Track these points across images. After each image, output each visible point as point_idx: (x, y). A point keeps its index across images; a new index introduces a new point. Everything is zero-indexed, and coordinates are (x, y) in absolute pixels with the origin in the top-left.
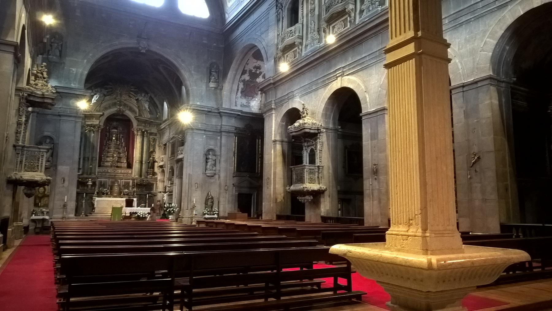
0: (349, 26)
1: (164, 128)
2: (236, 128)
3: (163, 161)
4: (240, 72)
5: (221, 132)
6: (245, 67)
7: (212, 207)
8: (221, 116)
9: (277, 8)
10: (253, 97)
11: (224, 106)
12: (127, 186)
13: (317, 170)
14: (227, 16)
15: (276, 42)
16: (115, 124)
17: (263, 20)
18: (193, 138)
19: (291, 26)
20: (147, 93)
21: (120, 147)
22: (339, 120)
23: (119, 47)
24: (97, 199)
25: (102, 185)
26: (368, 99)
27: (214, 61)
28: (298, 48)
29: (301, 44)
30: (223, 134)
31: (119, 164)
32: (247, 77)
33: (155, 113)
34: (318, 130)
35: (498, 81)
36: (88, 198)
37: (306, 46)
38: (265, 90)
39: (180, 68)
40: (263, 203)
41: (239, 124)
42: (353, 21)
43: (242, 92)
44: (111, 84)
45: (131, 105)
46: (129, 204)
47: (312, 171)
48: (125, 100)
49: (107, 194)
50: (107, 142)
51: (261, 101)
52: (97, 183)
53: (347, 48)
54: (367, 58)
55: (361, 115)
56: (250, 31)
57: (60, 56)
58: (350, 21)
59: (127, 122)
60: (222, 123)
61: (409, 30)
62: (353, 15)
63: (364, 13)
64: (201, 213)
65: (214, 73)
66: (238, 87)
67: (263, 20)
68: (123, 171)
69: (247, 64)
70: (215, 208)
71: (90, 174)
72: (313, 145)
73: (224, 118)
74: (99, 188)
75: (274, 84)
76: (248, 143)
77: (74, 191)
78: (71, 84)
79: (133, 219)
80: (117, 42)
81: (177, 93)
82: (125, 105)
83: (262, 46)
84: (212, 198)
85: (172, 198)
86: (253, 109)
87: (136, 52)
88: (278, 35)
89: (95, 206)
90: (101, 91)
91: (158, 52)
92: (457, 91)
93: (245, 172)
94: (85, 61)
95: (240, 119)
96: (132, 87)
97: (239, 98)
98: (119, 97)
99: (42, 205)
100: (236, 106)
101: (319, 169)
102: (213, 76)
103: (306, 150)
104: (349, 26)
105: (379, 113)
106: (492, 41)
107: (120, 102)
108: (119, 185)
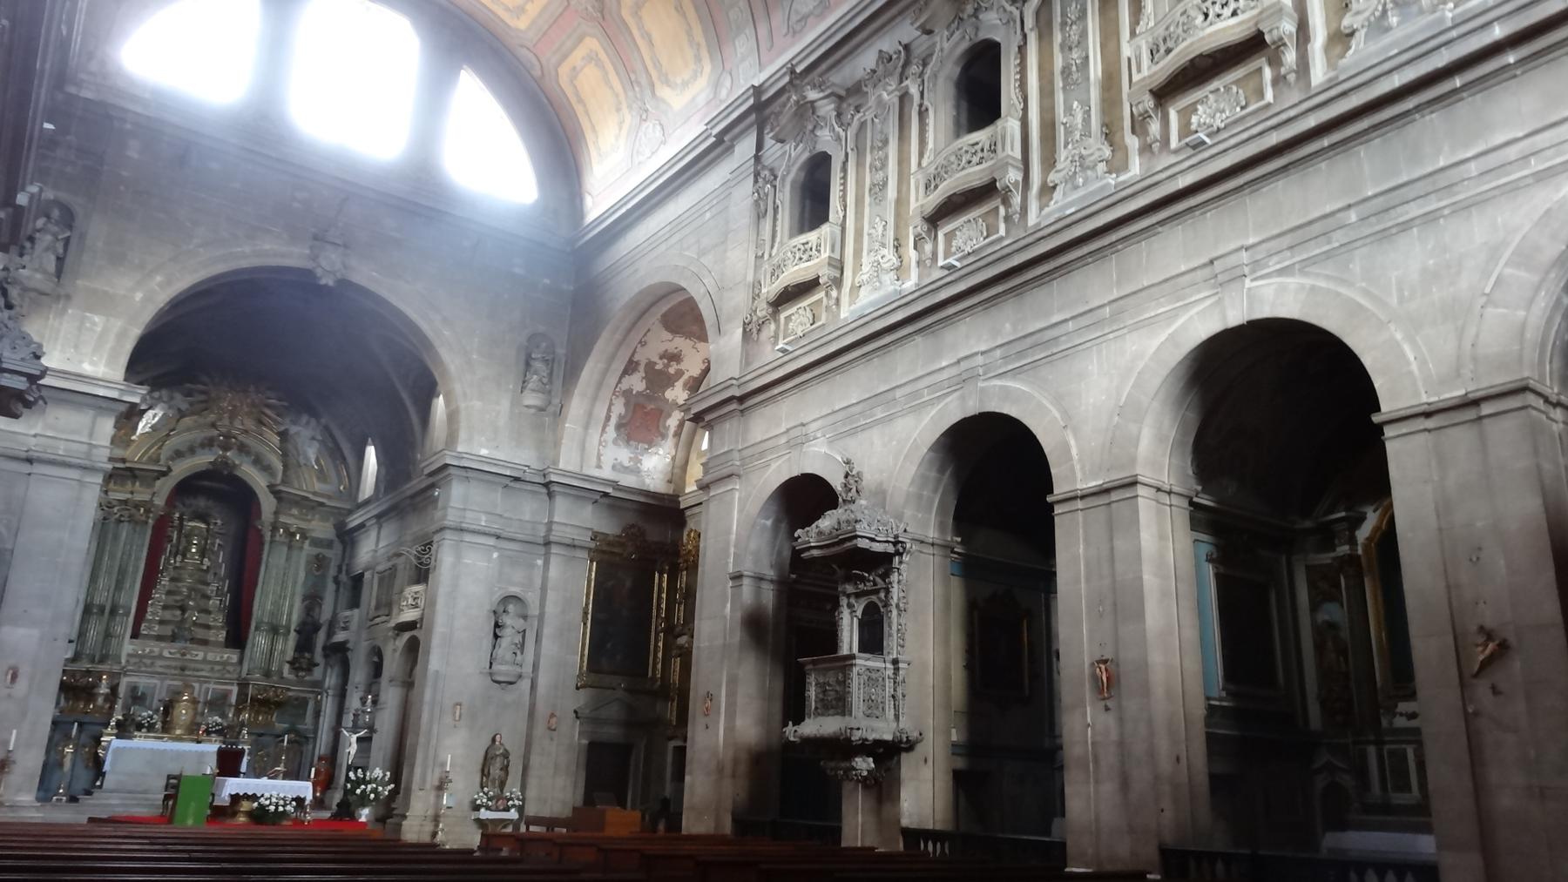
0: (1002, 232)
1: (362, 526)
3: (416, 606)
4: (619, 366)
5: (547, 544)
7: (502, 785)
8: (550, 495)
9: (756, 181)
10: (651, 444)
11: (561, 466)
13: (890, 672)
14: (588, 201)
15: (750, 278)
16: (201, 503)
17: (708, 215)
18: (458, 557)
19: (802, 231)
20: (313, 413)
22: (957, 518)
25: (137, 697)
26: (1074, 452)
27: (541, 328)
28: (827, 294)
29: (838, 282)
31: (200, 633)
32: (637, 383)
35: (1159, 490)
36: (84, 738)
37: (856, 289)
38: (707, 418)
39: (437, 343)
40: (687, 778)
41: (609, 526)
42: (1016, 217)
43: (619, 427)
44: (205, 379)
45: (264, 450)
46: (228, 764)
47: (874, 675)
48: (246, 432)
49: (151, 728)
50: (167, 560)
51: (673, 459)
52: (122, 690)
54: (1071, 325)
55: (1049, 499)
56: (663, 247)
57: (59, 273)
58: (1007, 219)
59: (240, 499)
60: (551, 514)
62: (1016, 200)
63: (1058, 195)
64: (466, 802)
65: (538, 365)
66: (609, 410)
67: (708, 215)
68: (210, 657)
69: (643, 343)
70: (513, 789)
71: (101, 661)
72: (876, 592)
73: (560, 503)
74: (126, 707)
75: (742, 399)
76: (628, 584)
77: (45, 708)
78: (81, 362)
79: (242, 819)
80: (247, 249)
81: (415, 419)
82: (243, 449)
83: (703, 290)
84: (506, 755)
85: (369, 750)
86: (648, 481)
87: (303, 281)
88: (759, 258)
89: (107, 767)
90: (172, 398)
91: (373, 287)
92: (1404, 428)
93: (614, 673)
94: (139, 296)
95: (611, 507)
96: (269, 393)
97: (610, 444)
98: (226, 422)
100: (599, 467)
101: (897, 670)
102: (536, 373)
103: (850, 606)
104: (1002, 232)
105: (1115, 496)
106: (1523, 274)
107: (228, 436)
108: (194, 702)
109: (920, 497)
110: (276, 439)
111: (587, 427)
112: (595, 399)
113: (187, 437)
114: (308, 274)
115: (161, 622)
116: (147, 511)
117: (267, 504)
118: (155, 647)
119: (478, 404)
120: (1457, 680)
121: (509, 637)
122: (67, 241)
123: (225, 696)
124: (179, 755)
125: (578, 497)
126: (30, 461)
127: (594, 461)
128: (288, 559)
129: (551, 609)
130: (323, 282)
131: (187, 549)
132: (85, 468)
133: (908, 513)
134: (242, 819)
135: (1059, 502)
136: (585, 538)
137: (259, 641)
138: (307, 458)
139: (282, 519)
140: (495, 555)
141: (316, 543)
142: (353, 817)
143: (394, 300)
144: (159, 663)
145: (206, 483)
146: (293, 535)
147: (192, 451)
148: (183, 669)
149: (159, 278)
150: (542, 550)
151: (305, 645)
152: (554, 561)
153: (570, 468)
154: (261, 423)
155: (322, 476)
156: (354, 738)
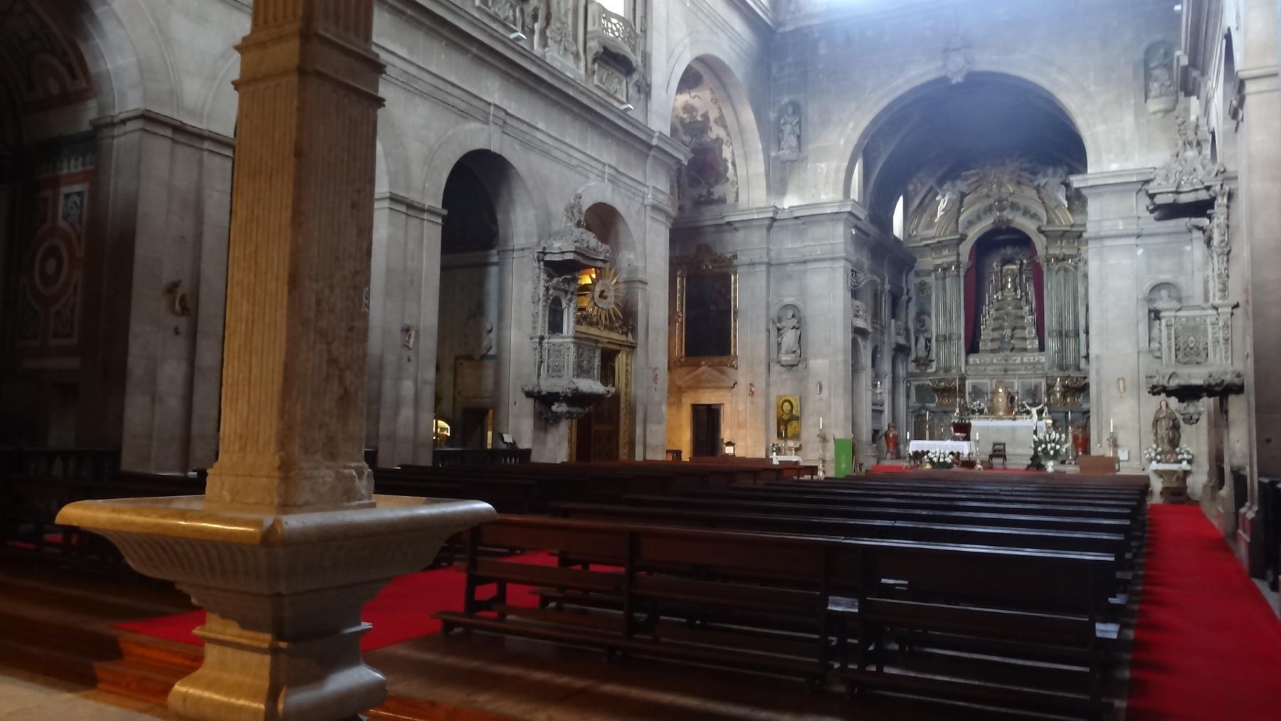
12: (1033, 394)
16: (1009, 251)
21: (1023, 303)
23: (907, 88)
31: (1018, 344)
34: (1208, 188)
49: (981, 412)
52: (968, 389)
53: (499, 69)
59: (1024, 241)
82: (1014, 207)
94: (842, 142)
114: (943, 80)
116: (958, 267)
117: (1039, 242)
118: (987, 358)
119: (1101, 128)
120: (200, 339)
122: (799, 123)
123: (1037, 387)
124: (999, 430)
126: (805, 262)
130: (954, 81)
131: (1006, 286)
132: (833, 259)
137: (1052, 344)
138: (1057, 200)
140: (1140, 252)
142: (1041, 467)
143: (1013, 72)
144: (989, 368)
147: (979, 218)
149: (851, 125)
154: (1019, 183)
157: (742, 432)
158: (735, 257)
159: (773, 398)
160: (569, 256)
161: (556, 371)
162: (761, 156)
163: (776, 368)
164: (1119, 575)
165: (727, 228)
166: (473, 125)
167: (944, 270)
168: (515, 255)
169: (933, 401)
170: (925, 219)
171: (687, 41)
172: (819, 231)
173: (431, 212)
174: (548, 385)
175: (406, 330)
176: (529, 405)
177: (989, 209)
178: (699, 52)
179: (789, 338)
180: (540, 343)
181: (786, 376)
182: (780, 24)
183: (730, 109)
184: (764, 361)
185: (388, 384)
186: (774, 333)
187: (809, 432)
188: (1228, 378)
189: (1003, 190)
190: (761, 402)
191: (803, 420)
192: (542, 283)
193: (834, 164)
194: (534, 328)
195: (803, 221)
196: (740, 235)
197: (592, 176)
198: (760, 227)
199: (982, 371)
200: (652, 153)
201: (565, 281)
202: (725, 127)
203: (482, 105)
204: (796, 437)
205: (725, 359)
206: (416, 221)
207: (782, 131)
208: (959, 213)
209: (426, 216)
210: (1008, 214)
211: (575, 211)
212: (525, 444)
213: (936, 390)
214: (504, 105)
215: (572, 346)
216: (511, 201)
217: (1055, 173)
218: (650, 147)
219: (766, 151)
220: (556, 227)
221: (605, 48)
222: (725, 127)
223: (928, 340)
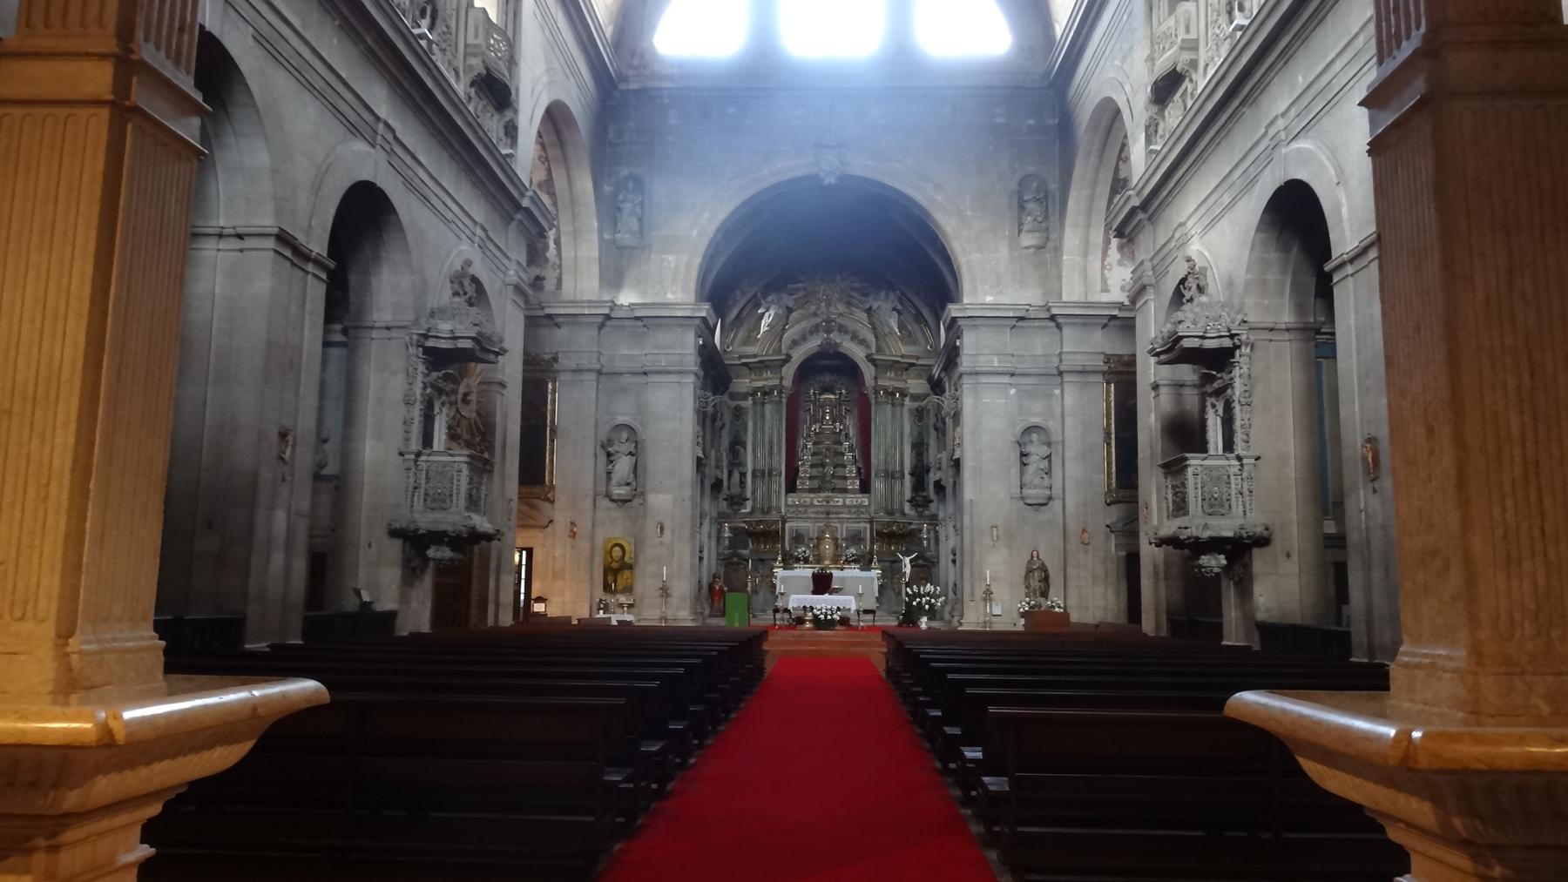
2: (1108, 359)
5: (1060, 374)
6: (1117, 170)
8: (1059, 327)
12: (855, 538)
13: (1235, 470)
16: (827, 378)
21: (842, 438)
23: (772, 181)
24: (779, 572)
25: (798, 538)
26: (1344, 211)
27: (1031, 169)
30: (1067, 378)
31: (839, 484)
33: (921, 339)
34: (1232, 336)
45: (858, 327)
59: (849, 369)
61: (147, 40)
68: (848, 502)
73: (1066, 330)
75: (1144, 206)
79: (808, 625)
84: (1044, 569)
94: (695, 233)
99: (620, 588)
103: (1214, 406)
107: (828, 321)
108: (835, 539)
109: (1264, 282)
110: (865, 315)
111: (1085, 254)
112: (1088, 225)
113: (804, 325)
115: (811, 478)
116: (780, 392)
117: (868, 371)
118: (807, 498)
119: (977, 256)
121: (1035, 463)
122: (642, 203)
125: (1085, 325)
127: (1099, 285)
128: (893, 415)
129: (1070, 434)
133: (1250, 302)
134: (808, 625)
135: (1342, 265)
136: (1099, 363)
137: (878, 485)
139: (880, 383)
140: (1013, 391)
141: (915, 398)
142: (915, 624)
145: (824, 362)
146: (893, 394)
147: (804, 338)
148: (828, 513)
149: (706, 215)
150: (1058, 380)
151: (919, 485)
152: (1067, 388)
153: (1075, 299)
154: (849, 304)
155: (908, 338)
156: (907, 560)
157: (559, 584)
158: (555, 359)
159: (599, 540)
160: (467, 344)
161: (438, 501)
162: (595, 237)
163: (605, 503)
164: (957, 731)
165: (545, 321)
166: (360, 146)
167: (765, 394)
168: (374, 334)
169: (746, 547)
170: (742, 333)
171: (545, 79)
172: (665, 337)
173: (317, 262)
174: (426, 520)
175: (283, 435)
176: (395, 546)
177: (815, 330)
178: (554, 98)
179: (623, 466)
180: (416, 461)
181: (617, 513)
182: (625, 79)
183: (563, 171)
184: (591, 493)
185: (261, 512)
186: (603, 459)
187: (646, 582)
188: (1259, 530)
189: (832, 309)
190: (584, 545)
191: (637, 569)
192: (420, 377)
193: (685, 258)
194: (407, 440)
195: (644, 322)
196: (563, 333)
197: (463, 237)
198: (590, 324)
199: (799, 512)
200: (518, 216)
201: (447, 377)
202: (552, 195)
203: (369, 118)
204: (629, 590)
205: (537, 489)
206: (300, 273)
207: (619, 209)
208: (784, 330)
209: (310, 267)
210: (835, 337)
211: (467, 282)
212: (386, 604)
213: (750, 534)
214: (391, 122)
215: (464, 467)
216: (376, 259)
217: (887, 296)
218: (518, 207)
219: (600, 231)
220: (433, 302)
221: (487, 69)
222: (552, 195)
223: (743, 475)
